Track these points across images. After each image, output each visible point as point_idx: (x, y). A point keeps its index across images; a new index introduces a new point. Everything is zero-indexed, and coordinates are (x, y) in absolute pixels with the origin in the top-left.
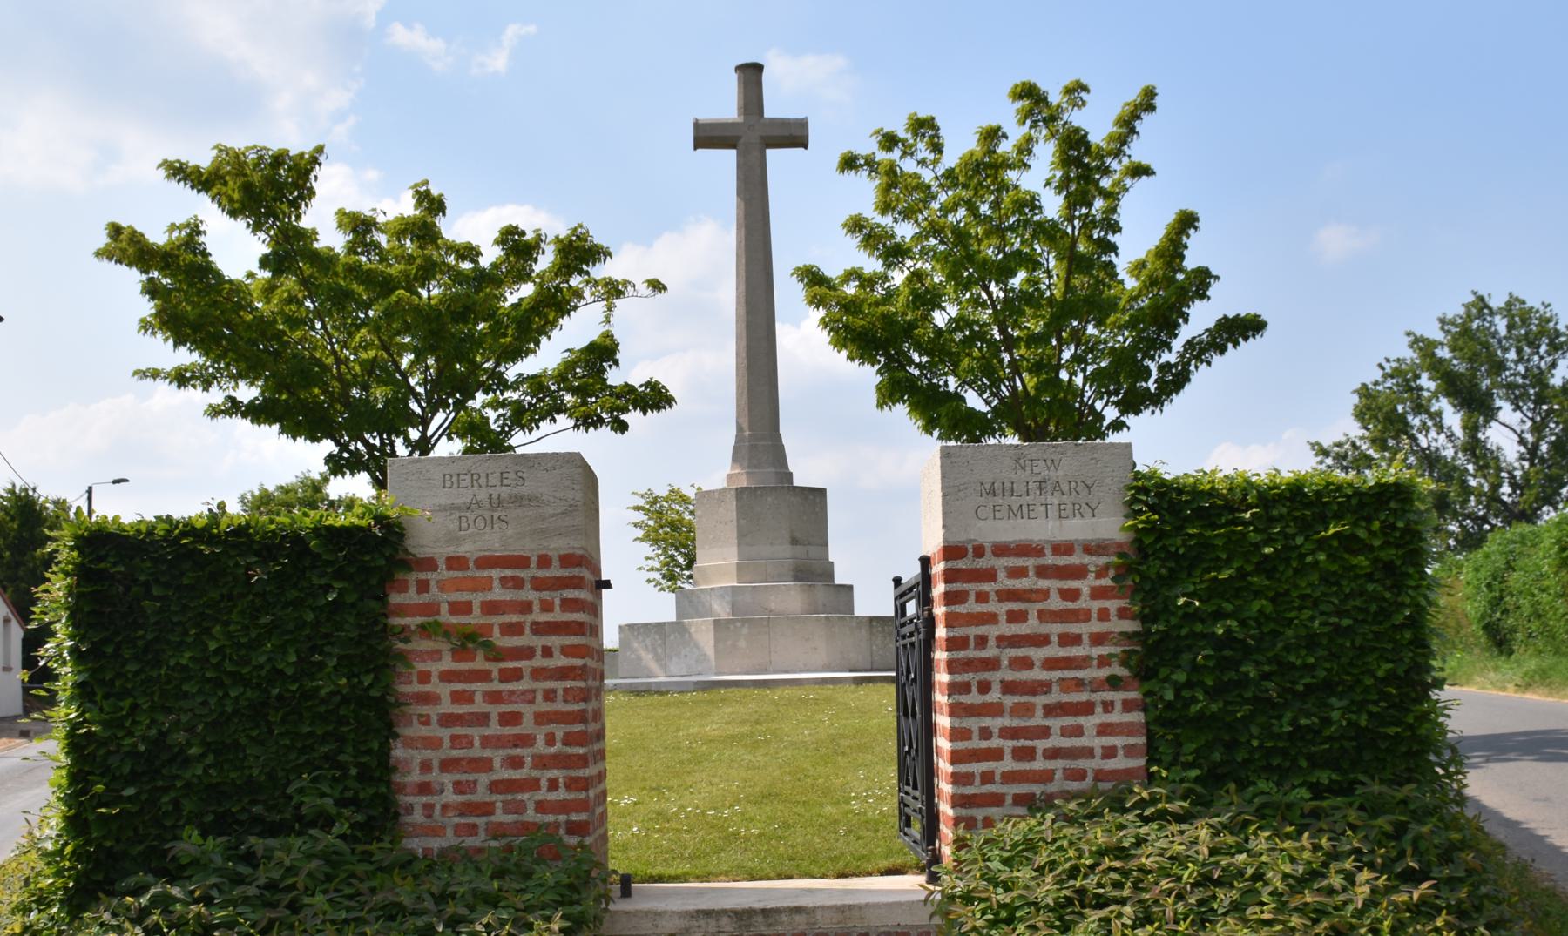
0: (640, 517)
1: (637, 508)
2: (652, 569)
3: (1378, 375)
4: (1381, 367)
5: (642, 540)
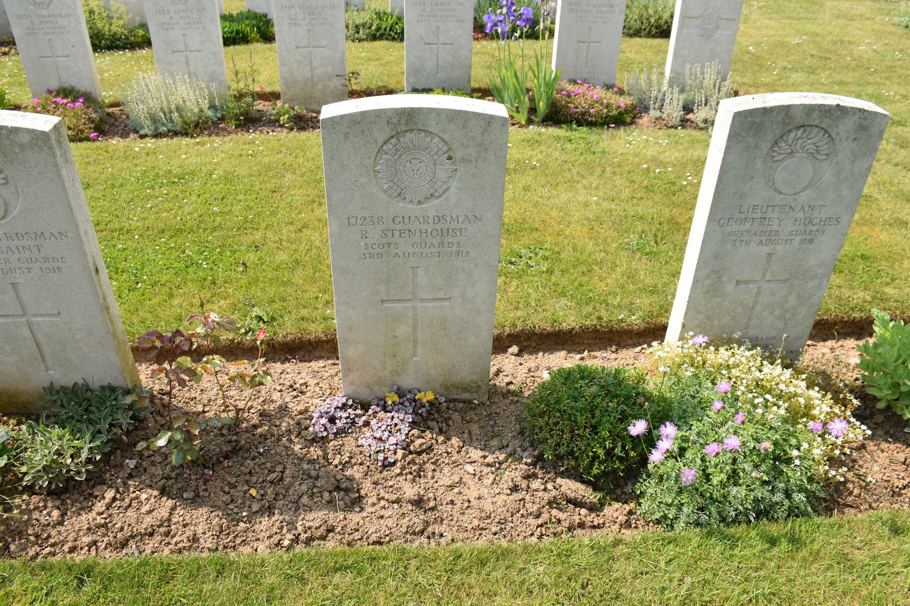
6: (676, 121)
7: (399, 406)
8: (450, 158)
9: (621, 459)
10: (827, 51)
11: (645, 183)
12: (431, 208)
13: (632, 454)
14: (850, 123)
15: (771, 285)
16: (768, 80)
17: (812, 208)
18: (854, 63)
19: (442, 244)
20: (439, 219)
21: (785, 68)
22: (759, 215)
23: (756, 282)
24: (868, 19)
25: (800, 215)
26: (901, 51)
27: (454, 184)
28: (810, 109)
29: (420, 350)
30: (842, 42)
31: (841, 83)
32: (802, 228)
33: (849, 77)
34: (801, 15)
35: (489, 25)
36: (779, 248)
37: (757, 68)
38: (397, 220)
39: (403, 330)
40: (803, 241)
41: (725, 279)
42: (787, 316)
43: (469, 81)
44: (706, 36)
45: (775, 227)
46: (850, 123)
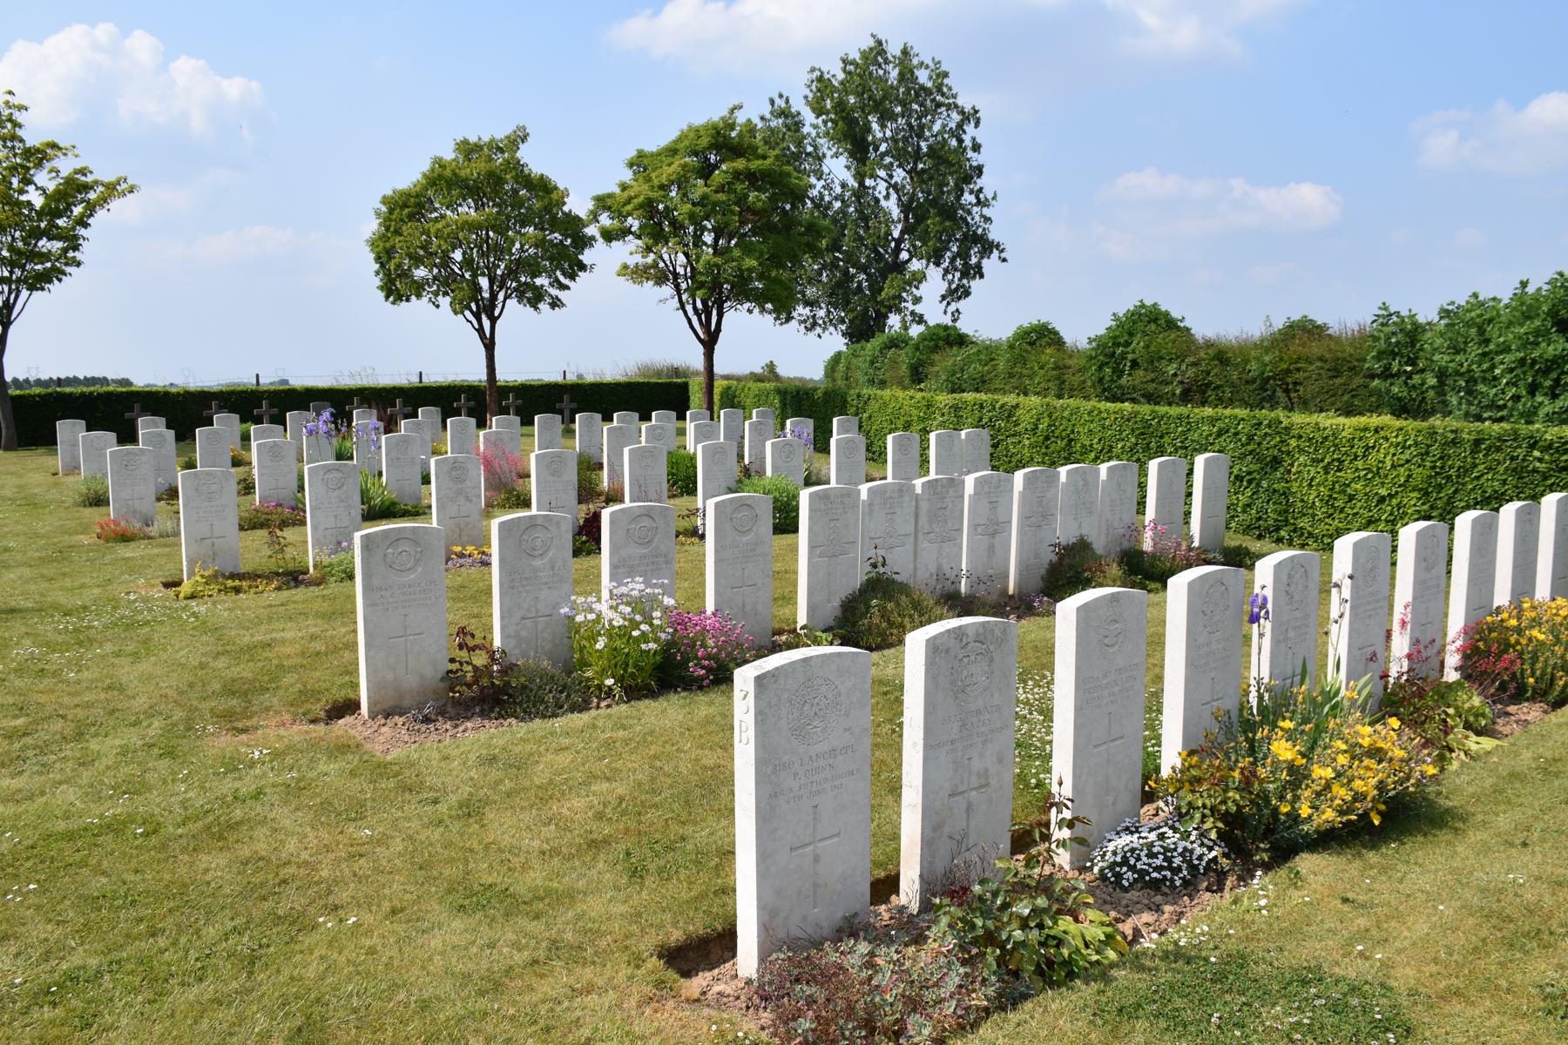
4: (772, 102)
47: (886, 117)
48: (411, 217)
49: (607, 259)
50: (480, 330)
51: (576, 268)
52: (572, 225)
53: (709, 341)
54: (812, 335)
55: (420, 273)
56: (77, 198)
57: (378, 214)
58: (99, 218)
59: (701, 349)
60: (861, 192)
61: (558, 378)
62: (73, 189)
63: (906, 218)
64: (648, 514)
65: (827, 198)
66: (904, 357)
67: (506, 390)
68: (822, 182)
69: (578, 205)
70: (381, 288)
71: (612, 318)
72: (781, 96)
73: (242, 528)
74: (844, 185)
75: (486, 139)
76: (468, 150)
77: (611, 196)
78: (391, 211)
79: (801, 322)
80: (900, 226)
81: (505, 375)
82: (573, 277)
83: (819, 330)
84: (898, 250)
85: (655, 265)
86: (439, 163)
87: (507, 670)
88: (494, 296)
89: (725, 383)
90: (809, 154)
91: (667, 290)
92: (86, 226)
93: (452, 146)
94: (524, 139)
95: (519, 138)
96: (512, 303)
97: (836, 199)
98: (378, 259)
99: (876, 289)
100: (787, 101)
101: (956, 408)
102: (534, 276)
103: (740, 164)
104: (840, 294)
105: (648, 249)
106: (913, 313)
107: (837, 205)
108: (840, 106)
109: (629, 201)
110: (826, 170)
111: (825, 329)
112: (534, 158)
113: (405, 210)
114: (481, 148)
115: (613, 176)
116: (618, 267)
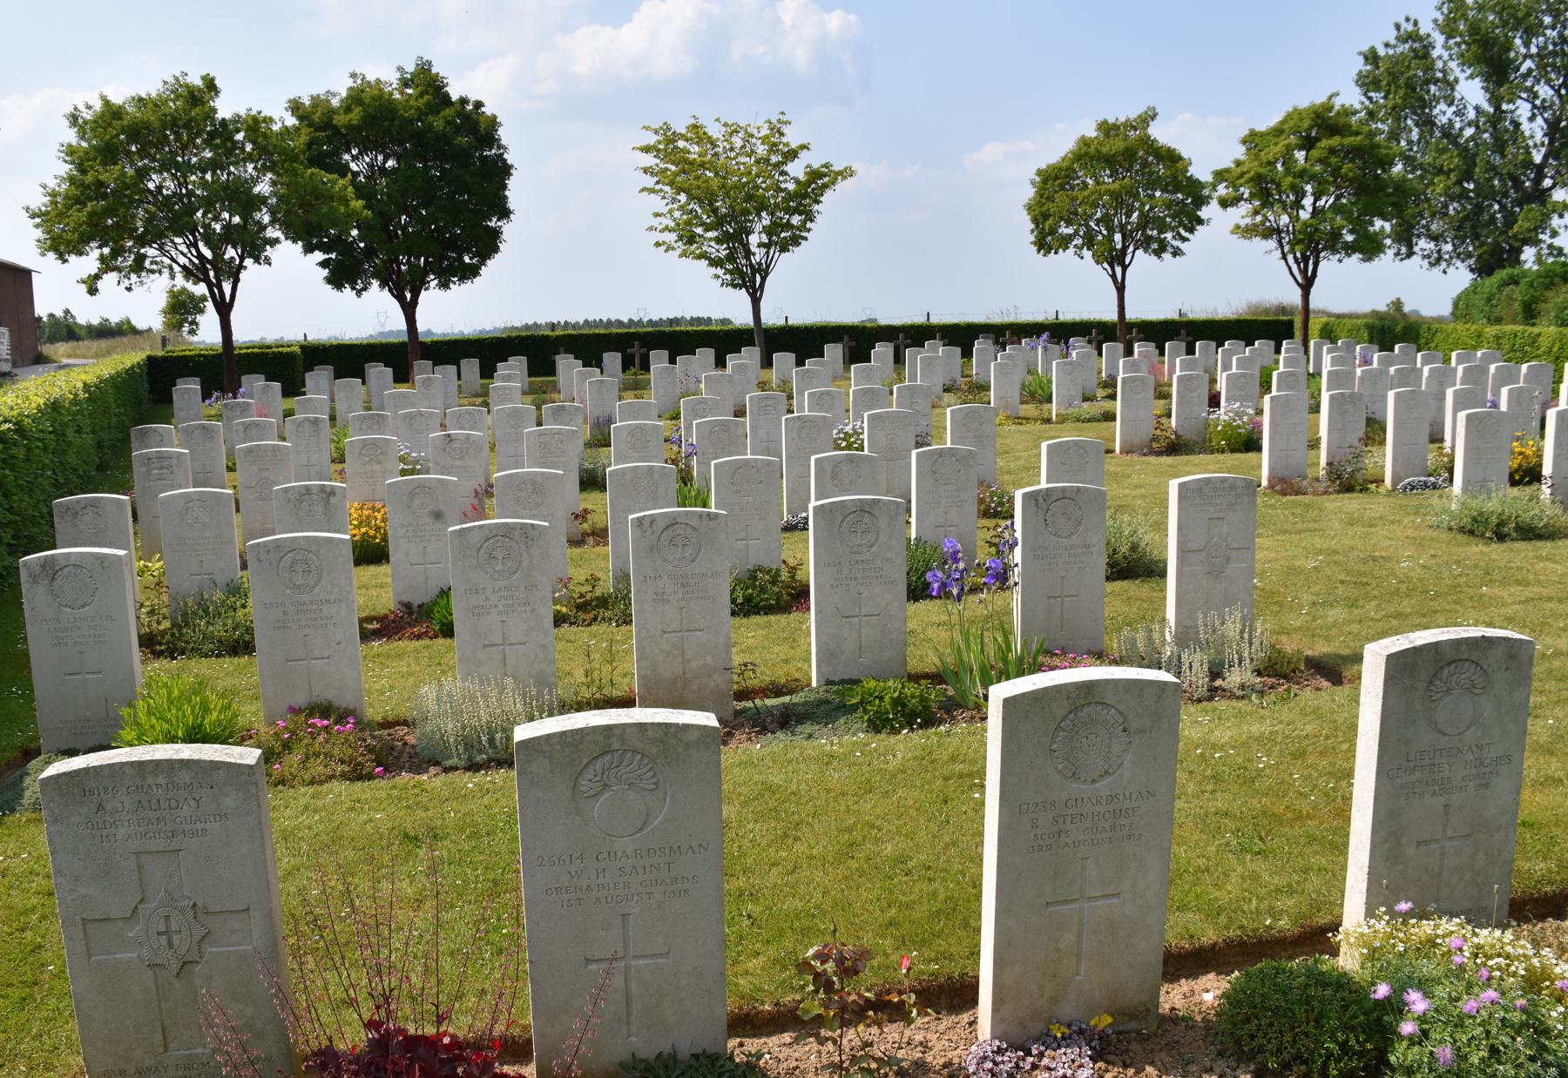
0: (650, 160)
1: (646, 149)
2: (667, 229)
3: (1391, 36)
4: (1398, 27)
5: (652, 191)
6: (1202, 691)
7: (1066, 1041)
8: (1125, 730)
9: (1361, 1054)
10: (1360, 574)
11: (1209, 772)
12: (1104, 787)
13: (1369, 1046)
14: (1497, 654)
15: (1454, 843)
16: (1298, 623)
17: (1480, 747)
18: (1404, 587)
19: (1113, 828)
20: (1112, 798)
21: (1314, 604)
22: (1427, 762)
23: (1437, 841)
24: (1393, 522)
25: (1470, 757)
26: (1458, 563)
27: (1129, 757)
28: (1457, 643)
29: (1084, 965)
30: (1375, 559)
31: (1398, 616)
32: (1473, 771)
33: (1406, 606)
34: (1299, 525)
35: (936, 586)
36: (1454, 797)
37: (1276, 608)
38: (1070, 803)
39: (1067, 940)
40: (1478, 787)
41: (1404, 840)
42: (1479, 880)
43: (905, 663)
44: (1215, 573)
45: (1446, 774)
46: (1497, 654)
47: (1530, 32)
48: (1062, 187)
49: (1219, 221)
50: (1114, 276)
51: (1194, 222)
52: (1196, 194)
53: (1307, 285)
54: (1436, 271)
55: (1066, 230)
56: (819, 181)
57: (1033, 183)
58: (828, 197)
59: (1299, 291)
60: (1497, 117)
61: (1176, 317)
62: (815, 175)
63: (1551, 142)
64: (1244, 375)
65: (1458, 125)
66: (1518, 293)
67: (1131, 326)
68: (1453, 108)
69: (1201, 171)
70: (1035, 243)
71: (1223, 266)
72: (1408, 20)
73: (366, 636)
74: (1477, 108)
75: (1122, 120)
76: (1107, 129)
77: (1227, 170)
78: (1045, 182)
79: (1424, 257)
80: (1543, 150)
81: (1132, 314)
82: (1191, 230)
83: (1444, 264)
84: (1540, 176)
85: (1263, 223)
86: (1084, 142)
87: (1178, 437)
88: (1125, 248)
89: (1325, 319)
90: (1438, 80)
91: (1272, 244)
92: (818, 202)
93: (1094, 126)
94: (1153, 118)
95: (1149, 117)
96: (1140, 252)
97: (1469, 124)
98: (1035, 220)
99: (1510, 219)
100: (1416, 23)
101: (1497, 338)
102: (1160, 232)
103: (1335, 141)
104: (1469, 228)
105: (1256, 213)
106: (1550, 246)
107: (1469, 132)
108: (1474, 29)
109: (1242, 175)
110: (1458, 96)
111: (1449, 263)
112: (1161, 133)
113: (1054, 181)
114: (1118, 127)
115: (1230, 153)
116: (1231, 227)
